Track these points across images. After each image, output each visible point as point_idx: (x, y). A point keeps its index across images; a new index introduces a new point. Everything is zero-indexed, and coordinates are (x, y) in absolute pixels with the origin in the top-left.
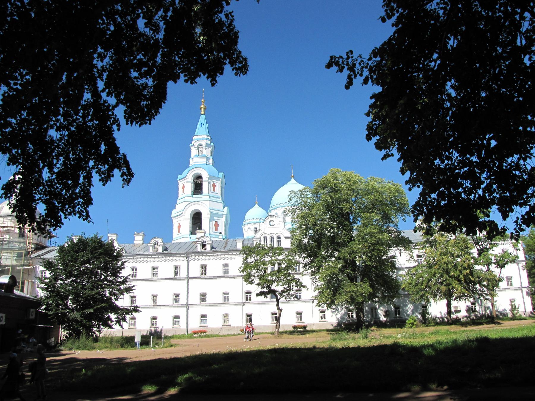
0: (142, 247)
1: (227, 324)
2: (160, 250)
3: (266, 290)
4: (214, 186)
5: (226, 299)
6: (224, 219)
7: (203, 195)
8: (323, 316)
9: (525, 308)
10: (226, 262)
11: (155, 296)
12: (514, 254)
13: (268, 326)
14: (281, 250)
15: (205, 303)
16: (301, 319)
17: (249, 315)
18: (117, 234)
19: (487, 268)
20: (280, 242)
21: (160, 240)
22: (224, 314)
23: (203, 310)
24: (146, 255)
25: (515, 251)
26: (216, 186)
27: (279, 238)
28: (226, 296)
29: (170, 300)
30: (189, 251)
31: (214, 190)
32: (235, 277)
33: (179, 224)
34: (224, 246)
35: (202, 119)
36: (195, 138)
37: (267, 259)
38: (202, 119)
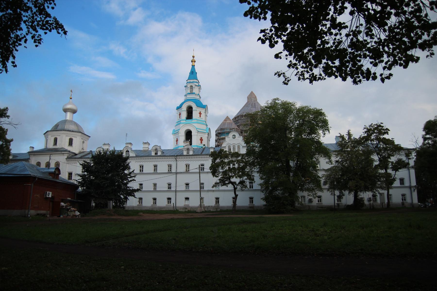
4: (200, 113)
7: (193, 119)
8: (404, 198)
12: (406, 161)
15: (188, 189)
16: (252, 202)
19: (385, 171)
23: (187, 195)
25: (407, 160)
31: (200, 116)
33: (177, 139)
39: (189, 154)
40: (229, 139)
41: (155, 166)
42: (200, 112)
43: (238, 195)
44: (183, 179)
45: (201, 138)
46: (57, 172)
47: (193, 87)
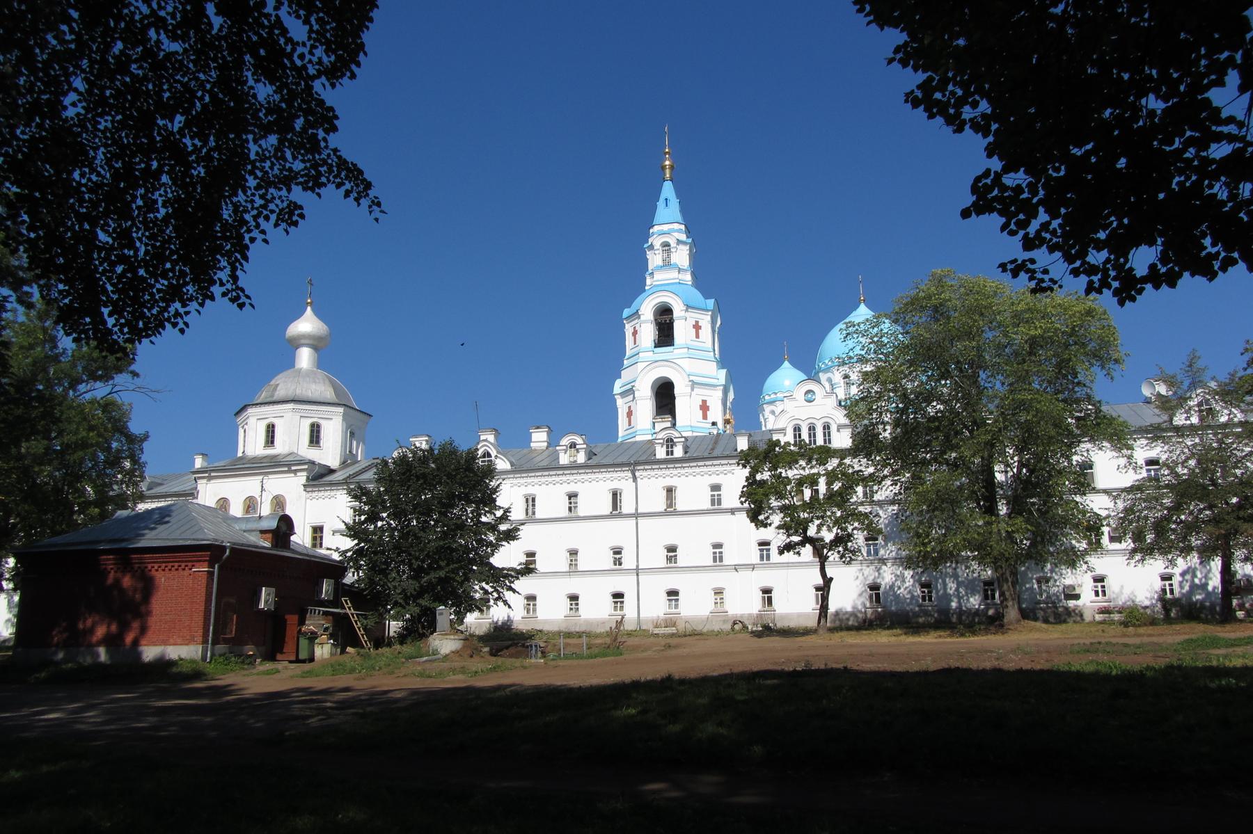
0: (546, 453)
1: (722, 610)
2: (581, 458)
3: (796, 539)
4: (697, 327)
5: (717, 558)
6: (719, 394)
9: (637, 524)
10: (715, 480)
11: (573, 553)
13: (806, 615)
14: (825, 453)
17: (767, 591)
18: (496, 430)
20: (829, 435)
21: (579, 440)
22: (714, 589)
23: (672, 581)
24: (553, 467)
26: (700, 328)
27: (827, 427)
28: (717, 550)
29: (607, 562)
30: (640, 459)
31: (697, 336)
32: (733, 511)
33: (630, 407)
34: (710, 447)
35: (668, 190)
36: (656, 229)
37: (792, 473)
38: (668, 190)
39: (672, 454)
40: (794, 403)
41: (572, 496)
42: (697, 322)
43: (831, 579)
44: (659, 533)
45: (704, 402)
46: (284, 528)
47: (669, 246)
